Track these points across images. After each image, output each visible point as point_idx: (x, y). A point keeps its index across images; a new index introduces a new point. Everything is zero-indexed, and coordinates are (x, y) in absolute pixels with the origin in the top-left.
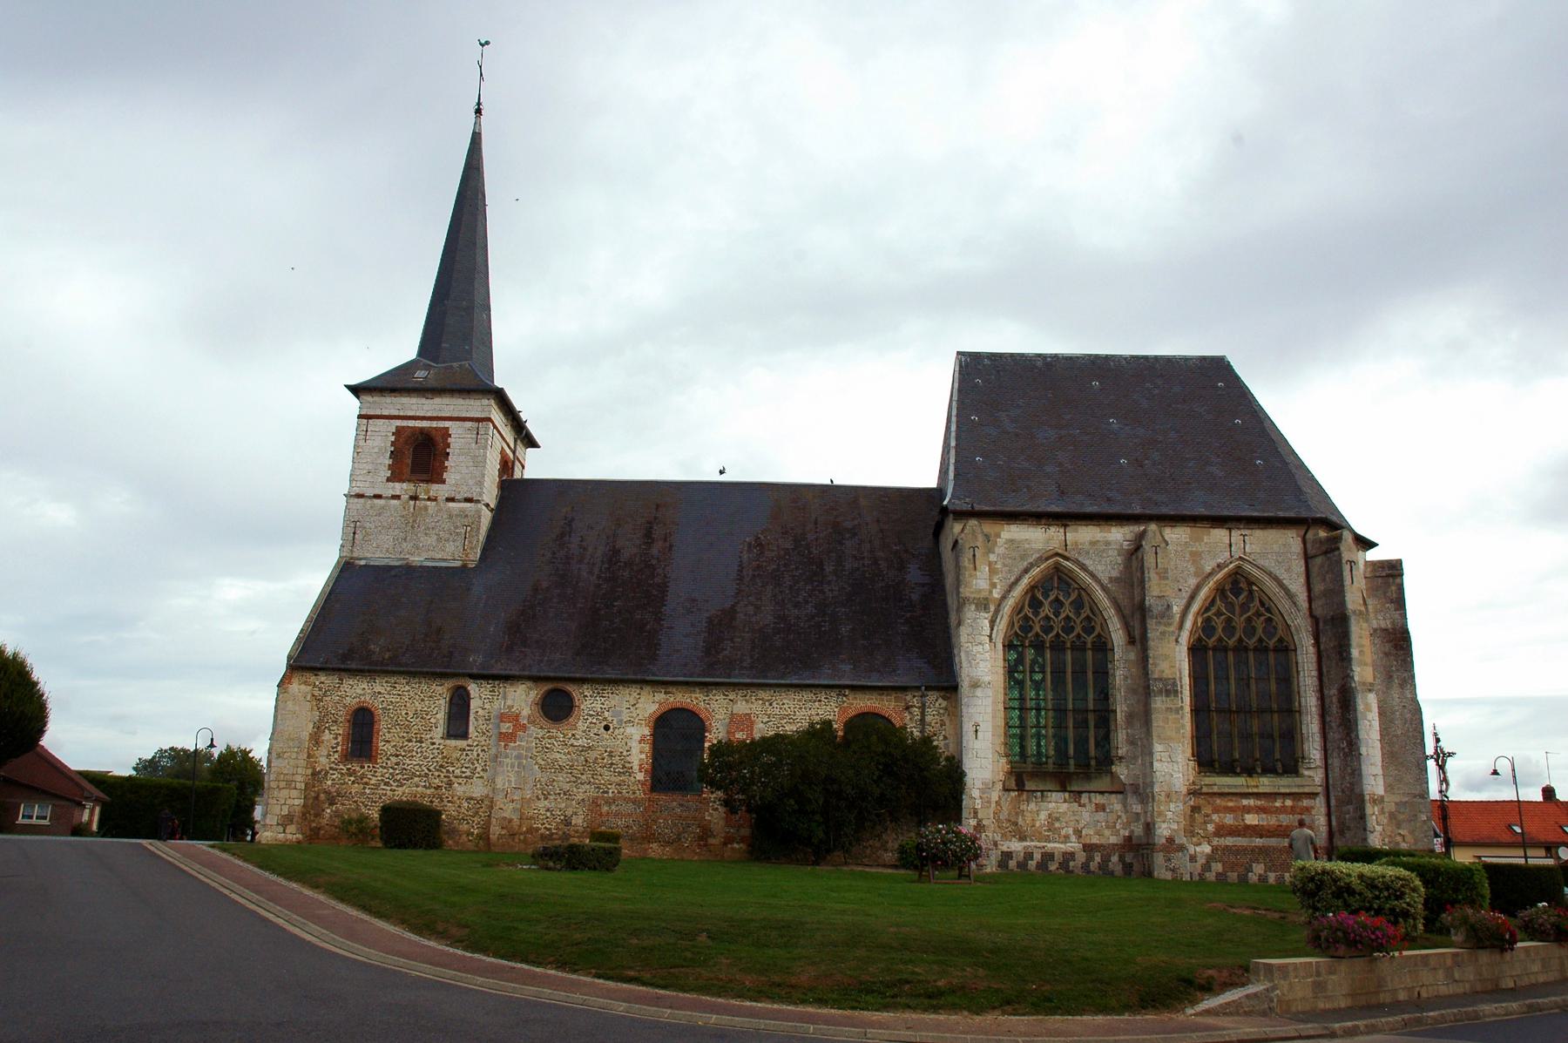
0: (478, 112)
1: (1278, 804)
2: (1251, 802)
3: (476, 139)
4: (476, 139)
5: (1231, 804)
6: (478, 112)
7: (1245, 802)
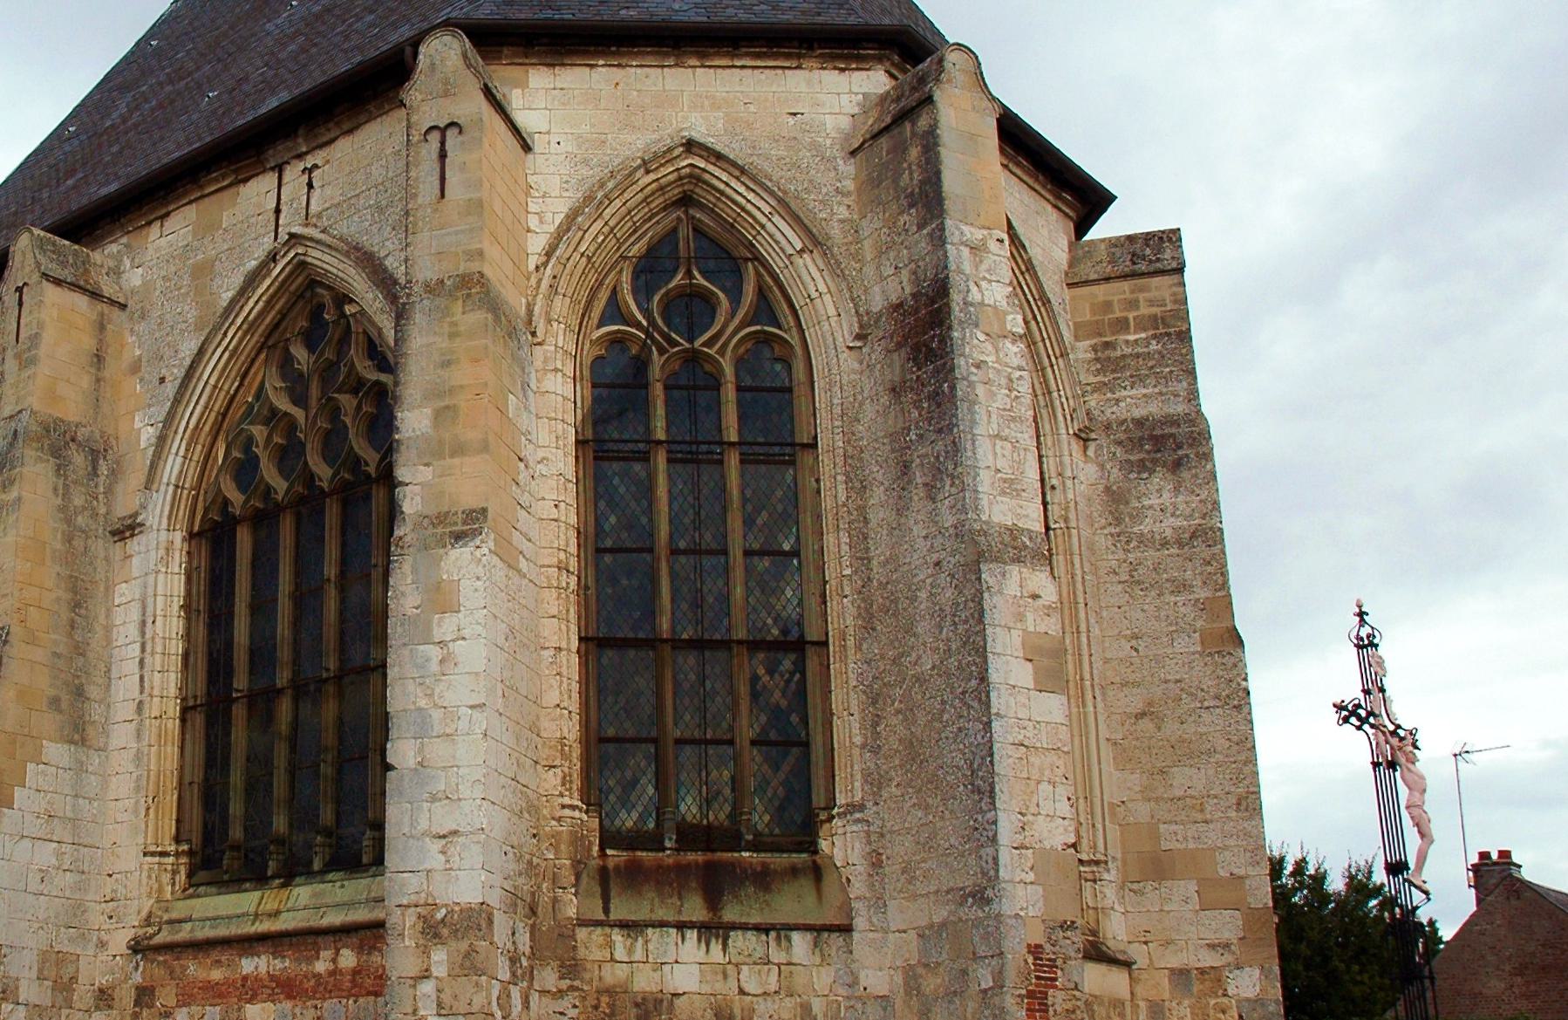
1: (321, 966)
2: (255, 965)
5: (217, 975)
7: (248, 965)
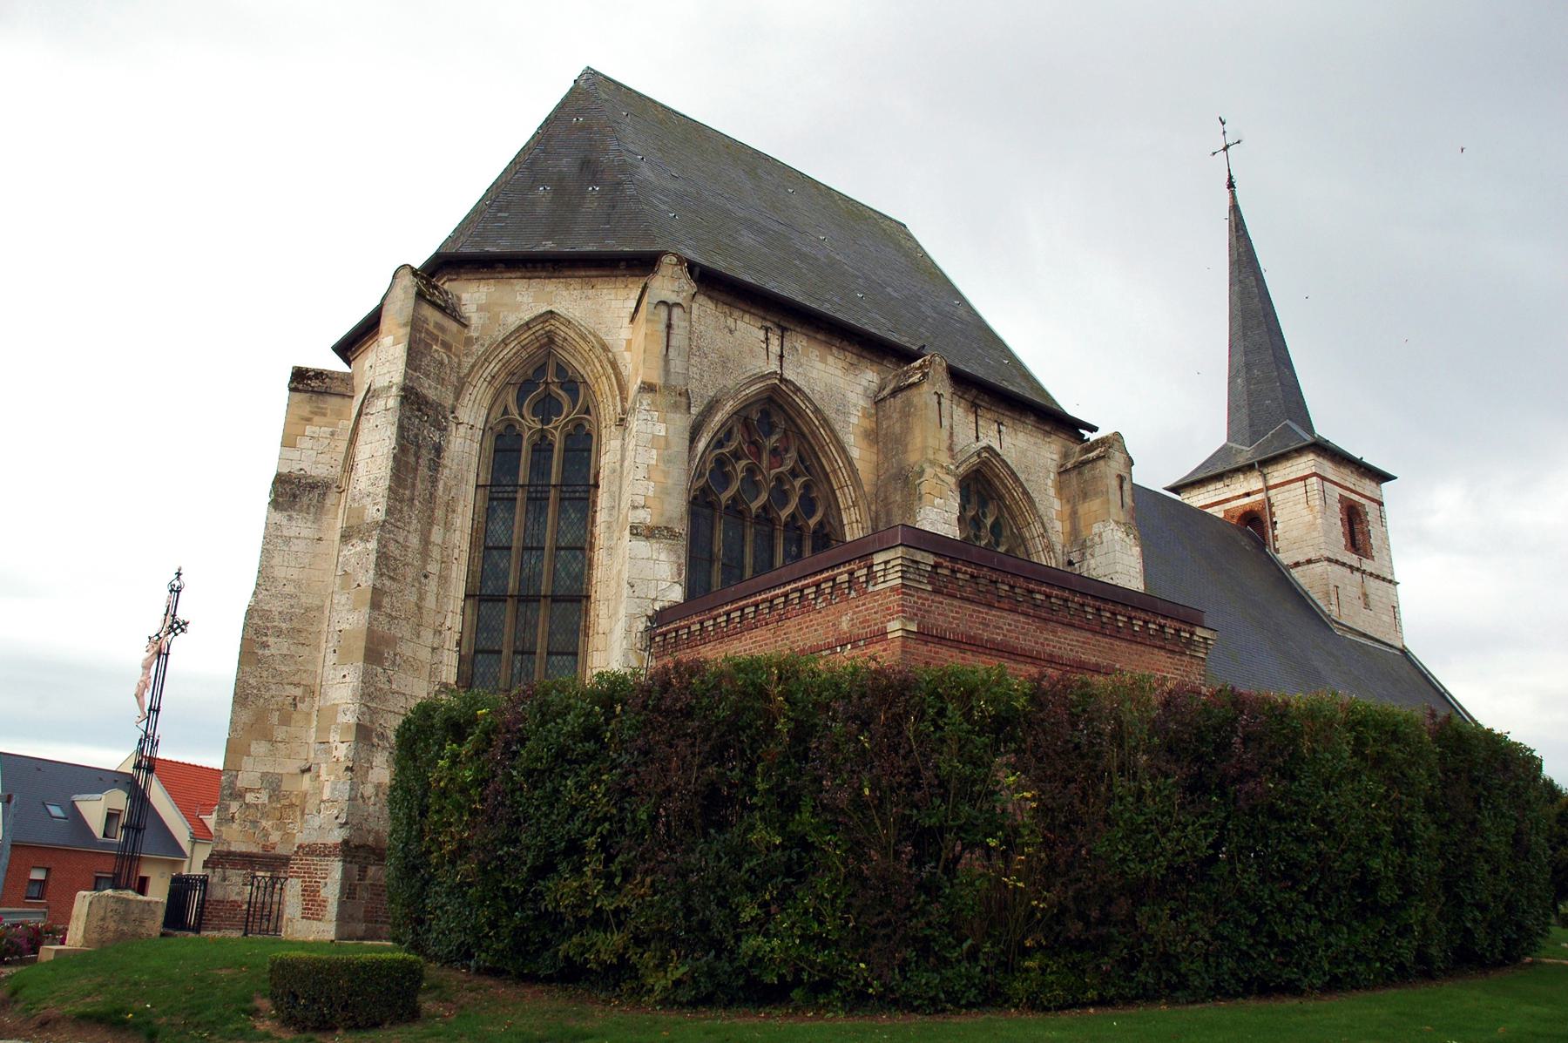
0: (1231, 185)
3: (1235, 208)
4: (1235, 208)
6: (1231, 185)
